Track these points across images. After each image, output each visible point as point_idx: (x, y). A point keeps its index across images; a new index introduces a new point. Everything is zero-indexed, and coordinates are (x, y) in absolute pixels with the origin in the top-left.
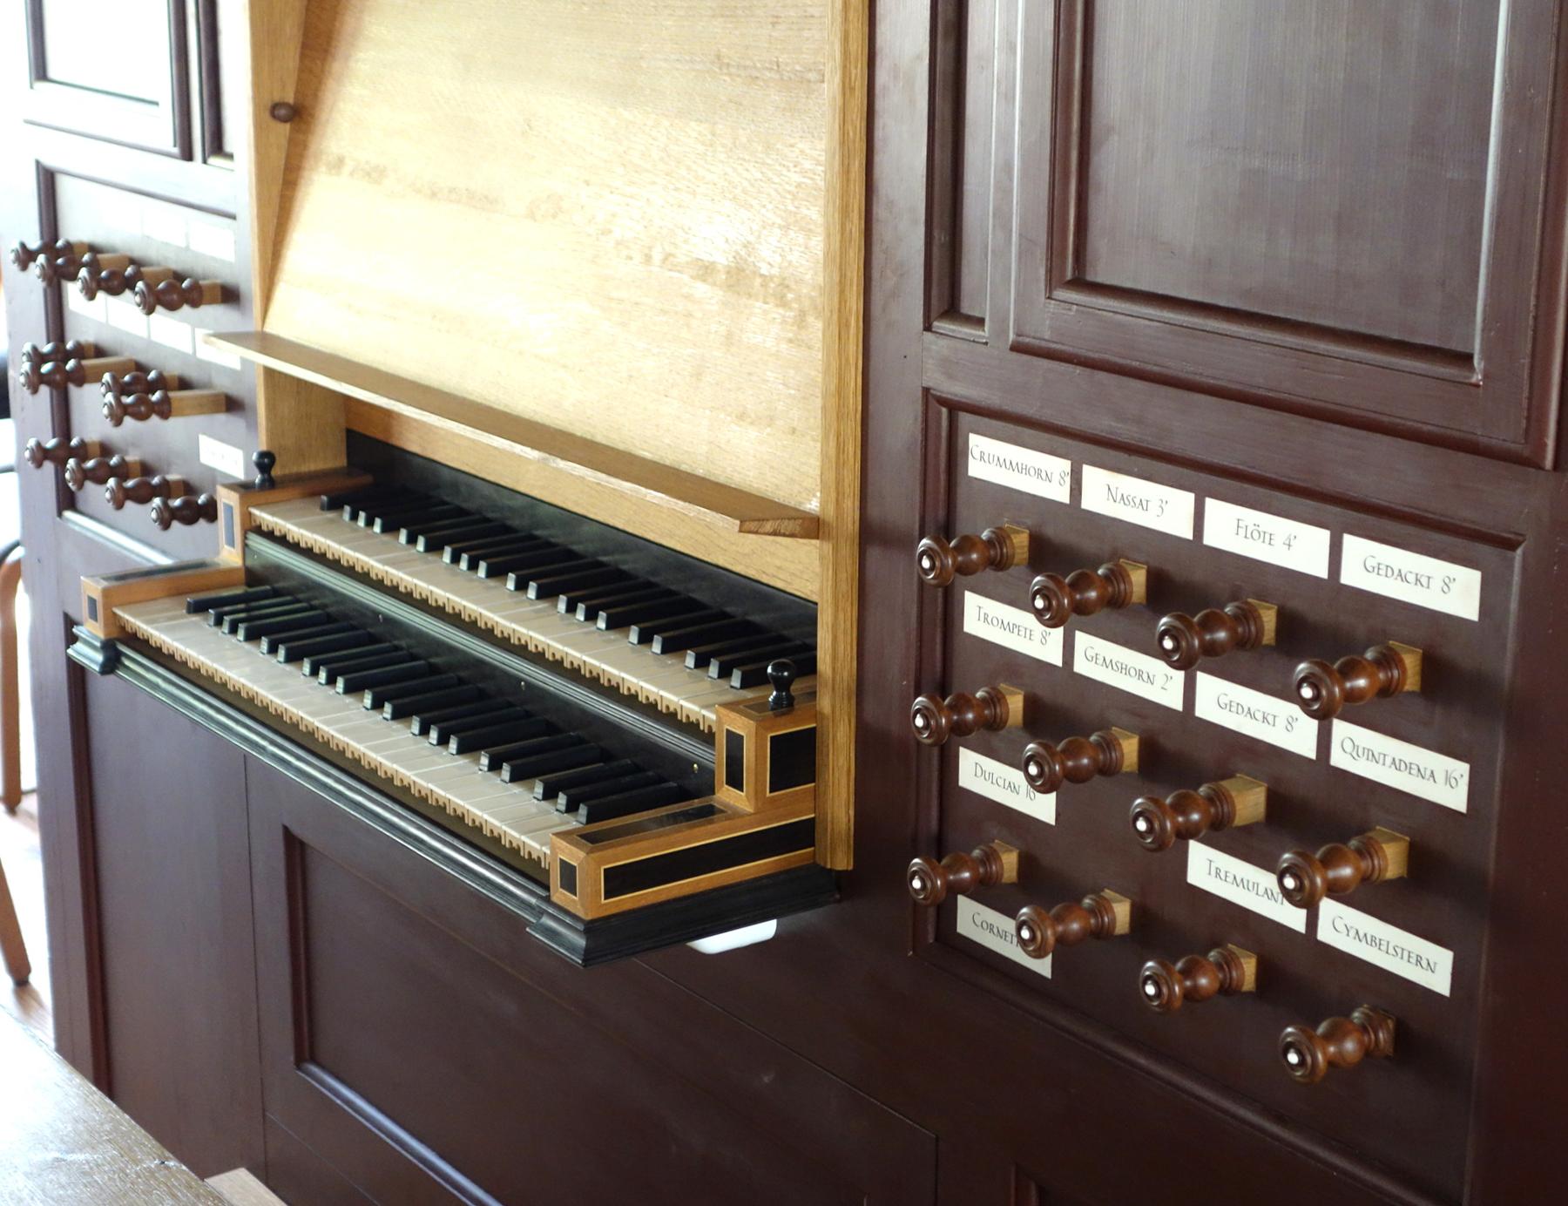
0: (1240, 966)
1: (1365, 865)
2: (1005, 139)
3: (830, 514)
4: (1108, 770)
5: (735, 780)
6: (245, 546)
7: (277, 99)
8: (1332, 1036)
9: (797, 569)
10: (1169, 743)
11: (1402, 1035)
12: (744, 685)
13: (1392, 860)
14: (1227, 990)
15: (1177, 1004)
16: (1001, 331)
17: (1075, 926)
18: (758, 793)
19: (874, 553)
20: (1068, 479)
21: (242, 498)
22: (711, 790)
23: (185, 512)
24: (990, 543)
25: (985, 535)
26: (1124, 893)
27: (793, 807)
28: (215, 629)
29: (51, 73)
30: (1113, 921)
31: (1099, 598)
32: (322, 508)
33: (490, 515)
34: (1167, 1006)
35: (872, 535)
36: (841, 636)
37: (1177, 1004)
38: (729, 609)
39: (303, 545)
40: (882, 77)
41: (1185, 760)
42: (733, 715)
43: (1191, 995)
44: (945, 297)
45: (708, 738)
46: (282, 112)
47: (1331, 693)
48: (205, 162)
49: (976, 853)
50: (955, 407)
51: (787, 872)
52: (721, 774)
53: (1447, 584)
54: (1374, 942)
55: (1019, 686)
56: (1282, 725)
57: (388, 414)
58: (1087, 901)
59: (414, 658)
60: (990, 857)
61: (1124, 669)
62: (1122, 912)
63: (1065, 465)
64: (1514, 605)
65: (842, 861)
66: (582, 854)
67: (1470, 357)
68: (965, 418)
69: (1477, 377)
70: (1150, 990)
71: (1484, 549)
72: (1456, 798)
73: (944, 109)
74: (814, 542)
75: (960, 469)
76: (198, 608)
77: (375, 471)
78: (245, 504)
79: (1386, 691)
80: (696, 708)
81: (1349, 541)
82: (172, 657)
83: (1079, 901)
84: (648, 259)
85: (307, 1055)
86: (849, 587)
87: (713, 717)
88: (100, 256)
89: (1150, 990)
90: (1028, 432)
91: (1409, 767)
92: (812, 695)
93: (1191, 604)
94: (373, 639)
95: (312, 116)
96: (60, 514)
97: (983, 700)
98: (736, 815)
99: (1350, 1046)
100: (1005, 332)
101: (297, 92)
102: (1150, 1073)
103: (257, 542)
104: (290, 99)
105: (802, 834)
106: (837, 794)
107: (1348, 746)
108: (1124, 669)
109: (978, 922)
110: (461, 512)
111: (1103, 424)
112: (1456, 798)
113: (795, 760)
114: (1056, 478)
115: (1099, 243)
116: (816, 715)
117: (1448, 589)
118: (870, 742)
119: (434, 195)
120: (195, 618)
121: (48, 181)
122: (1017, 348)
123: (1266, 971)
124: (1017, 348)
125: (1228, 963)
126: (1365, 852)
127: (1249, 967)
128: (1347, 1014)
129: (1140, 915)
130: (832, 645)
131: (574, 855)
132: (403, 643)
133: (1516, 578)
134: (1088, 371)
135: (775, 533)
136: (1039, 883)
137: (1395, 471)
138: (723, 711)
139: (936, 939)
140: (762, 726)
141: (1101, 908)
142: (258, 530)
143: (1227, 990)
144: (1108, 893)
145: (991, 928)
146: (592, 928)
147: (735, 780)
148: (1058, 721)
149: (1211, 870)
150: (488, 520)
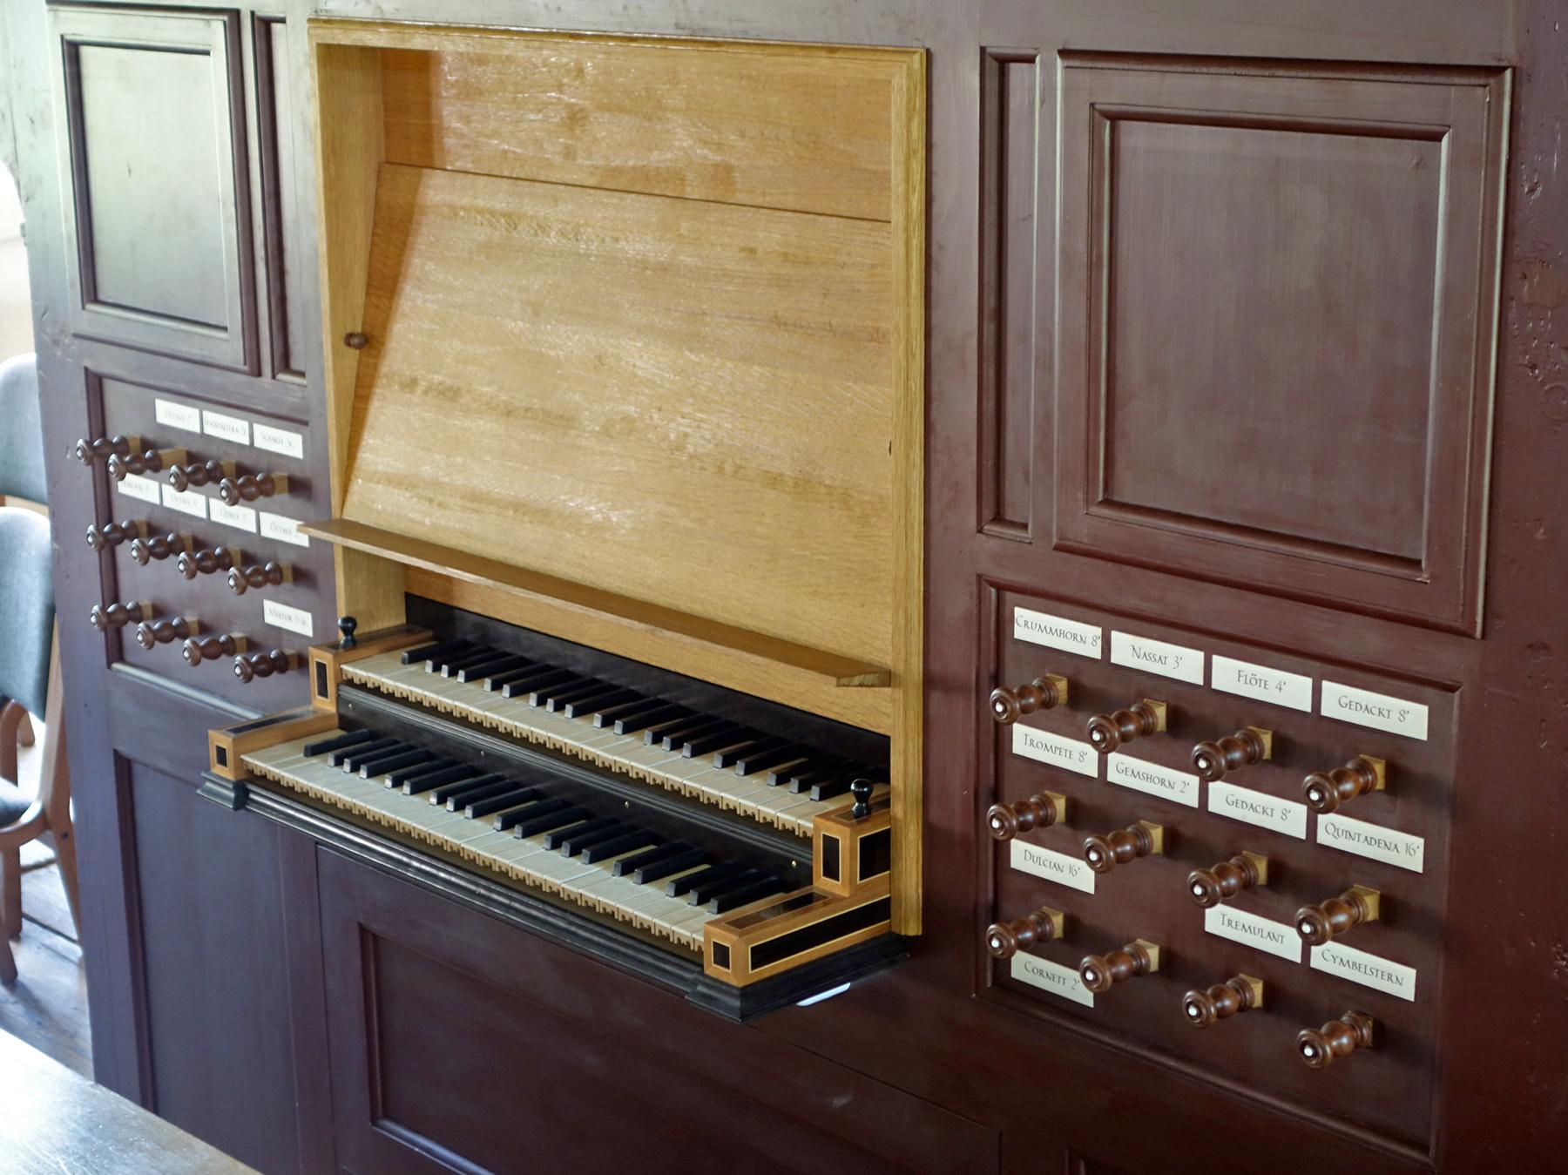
0: (1251, 990)
1: (1354, 911)
2: (1045, 395)
3: (899, 668)
4: (1141, 852)
5: (831, 871)
6: (338, 696)
7: (349, 330)
8: (1333, 1034)
9: (884, 712)
10: (1187, 831)
11: (1379, 1030)
12: (822, 798)
13: (1370, 907)
14: (1244, 1007)
15: (1213, 1020)
16: (1047, 534)
17: (1123, 968)
18: (852, 881)
19: (936, 696)
20: (1099, 642)
21: (335, 656)
22: (809, 880)
23: (262, 667)
24: (1041, 688)
25: (1035, 683)
26: (1153, 941)
27: (875, 889)
28: (337, 769)
29: (102, 297)
30: (1148, 962)
31: (1137, 729)
32: (404, 662)
33: (552, 663)
34: (1205, 1025)
35: (930, 682)
36: (910, 758)
37: (1213, 1020)
38: (598, 677)
39: (397, 695)
40: (936, 347)
41: (1195, 840)
42: (829, 824)
43: (1222, 1013)
44: (996, 511)
45: (807, 841)
46: (355, 341)
47: (1332, 795)
48: (274, 377)
49: (1032, 917)
50: (1001, 588)
51: (873, 939)
52: (818, 866)
53: (1403, 714)
54: (1355, 966)
55: (1062, 792)
56: (1283, 815)
57: (449, 579)
58: (1127, 949)
59: (517, 785)
60: (1044, 919)
61: (1150, 778)
62: (1153, 954)
63: (1098, 631)
64: (1455, 730)
65: (913, 929)
66: (735, 938)
67: (1418, 562)
68: (1009, 596)
69: (1424, 577)
70: (1193, 1011)
71: (1430, 692)
72: (1416, 865)
73: (990, 372)
74: (887, 690)
75: (1007, 631)
76: (314, 751)
77: (442, 632)
78: (338, 660)
79: (1365, 790)
80: (792, 819)
81: (1327, 685)
82: (306, 794)
83: (1121, 948)
84: (721, 470)
85: (380, 1113)
86: (916, 722)
87: (811, 825)
88: (161, 452)
89: (1193, 1011)
90: (1065, 607)
91: (1378, 842)
92: (886, 803)
93: (1192, 725)
94: (474, 772)
95: (383, 344)
96: (109, 666)
97: (1037, 804)
98: (838, 899)
99: (1345, 1040)
100: (1049, 535)
101: (364, 324)
102: (1181, 1072)
103: (348, 692)
104: (359, 330)
105: (881, 910)
106: (909, 875)
107: (1330, 829)
108: (1150, 778)
109: (1027, 968)
110: (524, 662)
111: (1131, 603)
112: (1416, 865)
113: (876, 854)
114: (1089, 640)
115: (1123, 474)
116: (890, 820)
117: (1407, 718)
118: (932, 836)
119: (509, 413)
120: (314, 760)
121: (96, 384)
122: (1058, 548)
123: (1270, 993)
124: (1058, 548)
125: (1242, 987)
126: (1354, 901)
127: (1257, 989)
128: (1338, 1018)
129: (1167, 957)
130: (904, 766)
131: (728, 939)
132: (506, 773)
133: (1456, 712)
134: (1117, 566)
135: (861, 685)
136: (1078, 938)
137: (1369, 640)
138: (820, 820)
139: (994, 983)
140: (854, 833)
141: (1139, 953)
142: (350, 683)
143: (1244, 1007)
144: (1140, 941)
145: (1041, 972)
146: (747, 992)
147: (831, 871)
148: (1091, 814)
149: (1222, 921)
150: (549, 668)
